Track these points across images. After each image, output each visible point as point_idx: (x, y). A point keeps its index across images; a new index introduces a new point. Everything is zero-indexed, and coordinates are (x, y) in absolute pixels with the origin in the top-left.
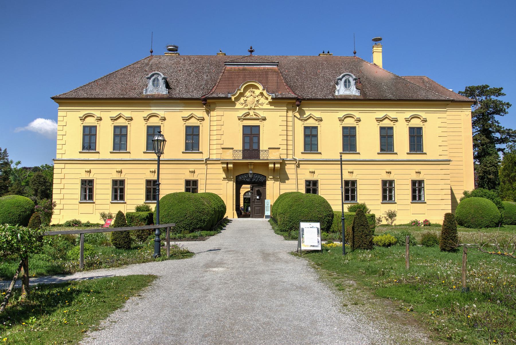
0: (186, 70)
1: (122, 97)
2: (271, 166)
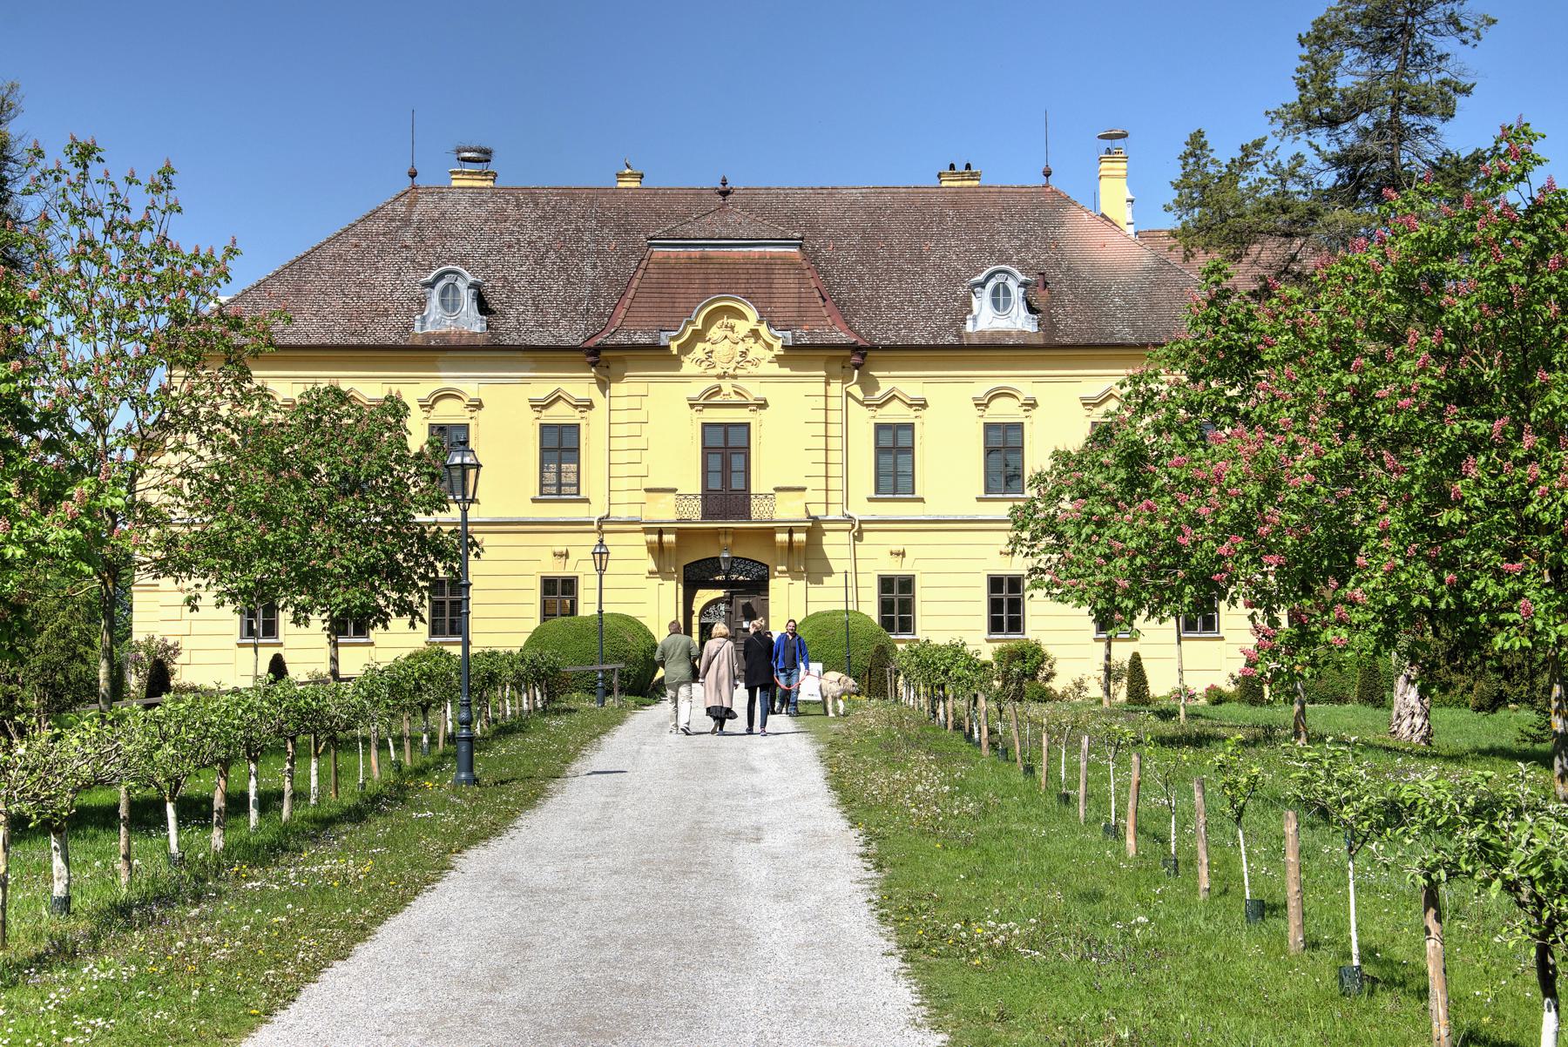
0: (529, 243)
1: (354, 341)
2: (782, 537)
